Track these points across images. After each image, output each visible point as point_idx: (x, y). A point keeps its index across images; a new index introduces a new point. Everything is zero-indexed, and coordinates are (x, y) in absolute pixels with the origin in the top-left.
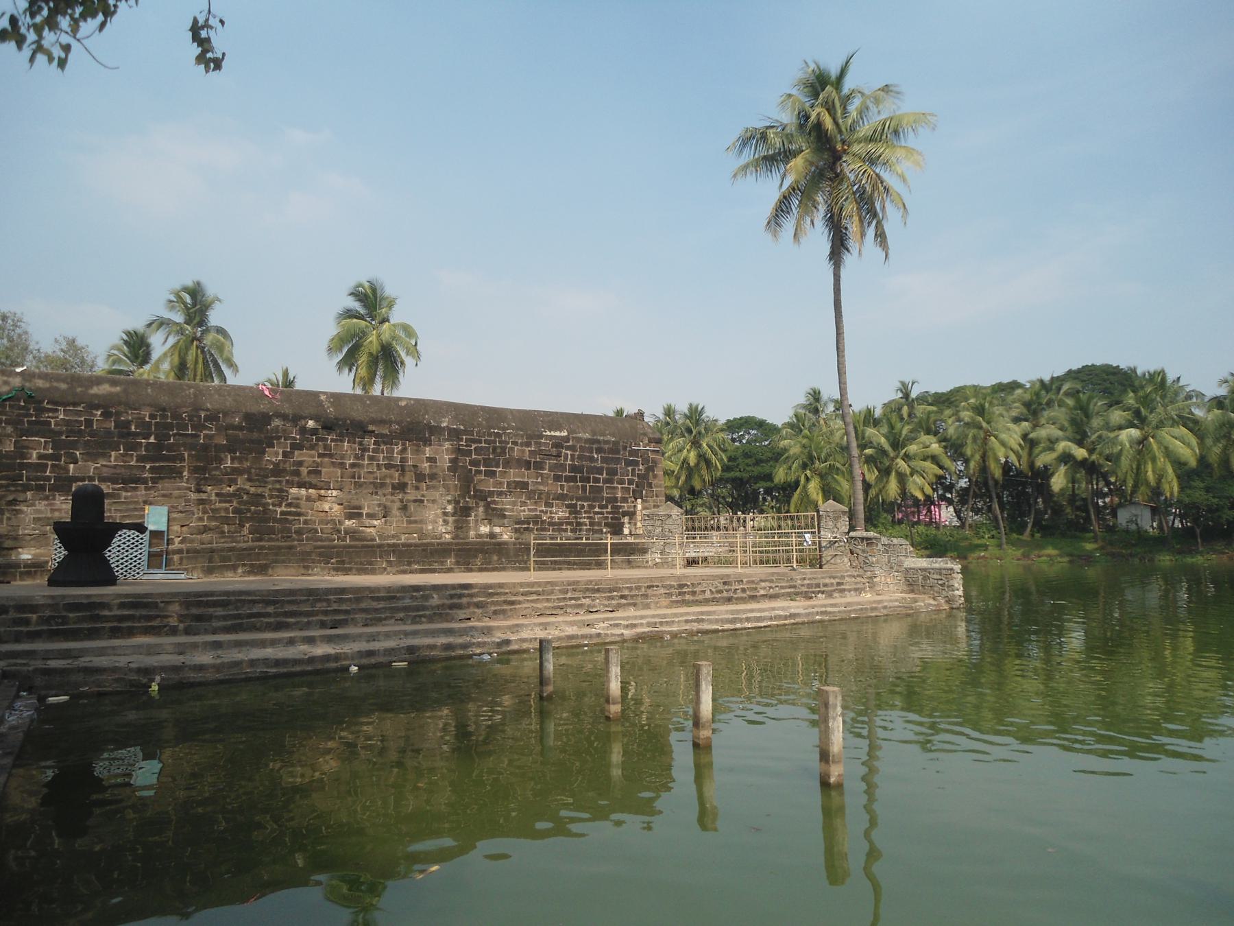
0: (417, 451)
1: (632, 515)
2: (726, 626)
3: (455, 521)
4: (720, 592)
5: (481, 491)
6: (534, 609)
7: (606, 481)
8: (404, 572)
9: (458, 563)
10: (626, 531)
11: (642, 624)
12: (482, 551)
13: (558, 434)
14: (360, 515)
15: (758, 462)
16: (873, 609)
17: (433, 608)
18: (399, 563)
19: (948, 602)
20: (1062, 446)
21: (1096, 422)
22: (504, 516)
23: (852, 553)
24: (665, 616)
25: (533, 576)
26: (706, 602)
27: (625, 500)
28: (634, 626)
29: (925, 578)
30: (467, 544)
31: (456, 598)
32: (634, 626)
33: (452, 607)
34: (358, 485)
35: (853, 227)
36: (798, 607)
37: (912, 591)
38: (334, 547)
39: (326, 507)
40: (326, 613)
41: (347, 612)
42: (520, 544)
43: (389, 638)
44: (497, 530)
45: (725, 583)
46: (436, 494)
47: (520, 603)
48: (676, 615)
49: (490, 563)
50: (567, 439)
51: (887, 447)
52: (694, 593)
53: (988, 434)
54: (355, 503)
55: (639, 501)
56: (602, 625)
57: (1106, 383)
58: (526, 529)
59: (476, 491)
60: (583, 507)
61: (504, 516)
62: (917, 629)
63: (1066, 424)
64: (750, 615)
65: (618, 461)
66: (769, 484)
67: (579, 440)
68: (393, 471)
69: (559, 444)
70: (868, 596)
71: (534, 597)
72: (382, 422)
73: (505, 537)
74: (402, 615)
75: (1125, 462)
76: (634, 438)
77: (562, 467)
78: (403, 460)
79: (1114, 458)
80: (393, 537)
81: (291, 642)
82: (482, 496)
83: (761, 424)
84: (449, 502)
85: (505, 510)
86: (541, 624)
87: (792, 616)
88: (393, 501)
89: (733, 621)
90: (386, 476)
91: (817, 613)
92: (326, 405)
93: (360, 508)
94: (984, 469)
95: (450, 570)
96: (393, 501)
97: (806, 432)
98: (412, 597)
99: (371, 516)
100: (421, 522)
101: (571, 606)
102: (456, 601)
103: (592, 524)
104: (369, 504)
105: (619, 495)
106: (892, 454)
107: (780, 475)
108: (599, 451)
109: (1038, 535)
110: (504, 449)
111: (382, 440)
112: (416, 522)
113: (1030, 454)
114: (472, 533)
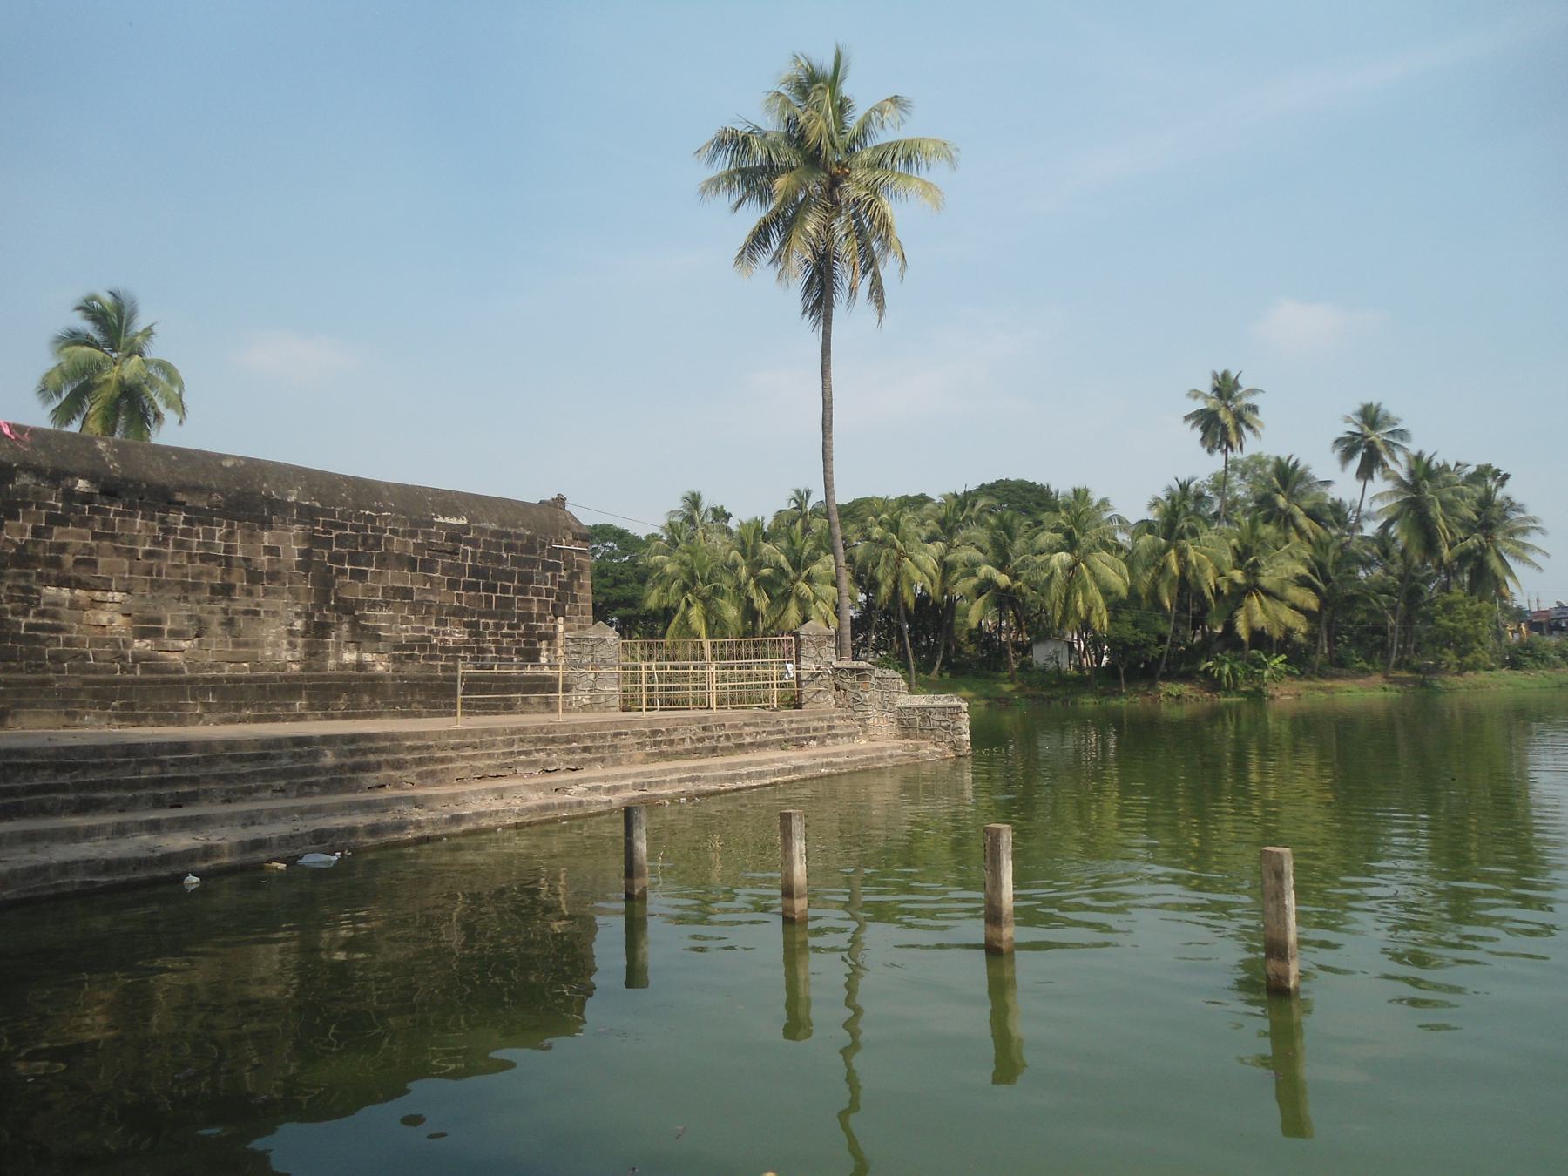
0: (251, 537)
1: (551, 638)
2: (728, 786)
3: (307, 645)
4: (701, 740)
5: (345, 600)
6: (473, 769)
7: (519, 591)
8: (231, 721)
9: (311, 707)
10: (543, 660)
11: (626, 786)
12: (346, 689)
13: (454, 521)
14: (159, 632)
15: (617, 583)
16: (880, 758)
17: (327, 770)
18: (223, 706)
19: (954, 748)
20: (985, 570)
21: (1019, 544)
22: (378, 638)
23: (837, 688)
24: (650, 774)
25: (460, 722)
26: (687, 754)
27: (542, 618)
28: (616, 789)
29: (924, 719)
30: (324, 678)
31: (359, 759)
32: (616, 789)
33: (357, 768)
34: (157, 586)
35: (844, 274)
36: (795, 757)
37: (907, 736)
38: (117, 682)
39: (103, 618)
40: (160, 782)
41: (193, 781)
42: (402, 678)
43: (277, 819)
44: (368, 657)
45: (705, 729)
46: (278, 603)
47: (451, 760)
48: (664, 772)
49: (358, 706)
50: (466, 529)
51: (787, 566)
52: (671, 742)
53: (902, 554)
54: (150, 612)
55: (561, 619)
56: (576, 789)
57: (1021, 502)
58: (409, 657)
59: (338, 599)
60: (487, 626)
61: (378, 638)
62: (914, 783)
63: (987, 546)
64: (752, 769)
65: (533, 563)
66: (630, 611)
67: (482, 531)
68: (212, 565)
69: (455, 535)
70: (862, 743)
71: (469, 752)
72: (197, 489)
73: (379, 668)
74: (282, 783)
75: (1055, 591)
76: (556, 534)
77: (460, 569)
78: (229, 549)
79: (1041, 588)
80: (211, 667)
81: (121, 831)
82: (347, 608)
83: (621, 535)
84: (298, 615)
85: (379, 628)
86: (495, 790)
87: (797, 769)
88: (212, 612)
89: (733, 778)
90: (201, 574)
91: (823, 765)
92: (108, 457)
93: (159, 621)
94: (896, 592)
95: (300, 718)
96: (212, 612)
97: (682, 545)
98: (295, 756)
99: (177, 634)
100: (256, 644)
101: (522, 763)
102: (357, 759)
103: (498, 651)
104: (173, 615)
105: (535, 611)
106: (792, 575)
107: (652, 599)
108: (509, 548)
109: (947, 675)
110: (378, 539)
111: (197, 517)
112: (246, 644)
113: (943, 580)
114: (331, 663)
